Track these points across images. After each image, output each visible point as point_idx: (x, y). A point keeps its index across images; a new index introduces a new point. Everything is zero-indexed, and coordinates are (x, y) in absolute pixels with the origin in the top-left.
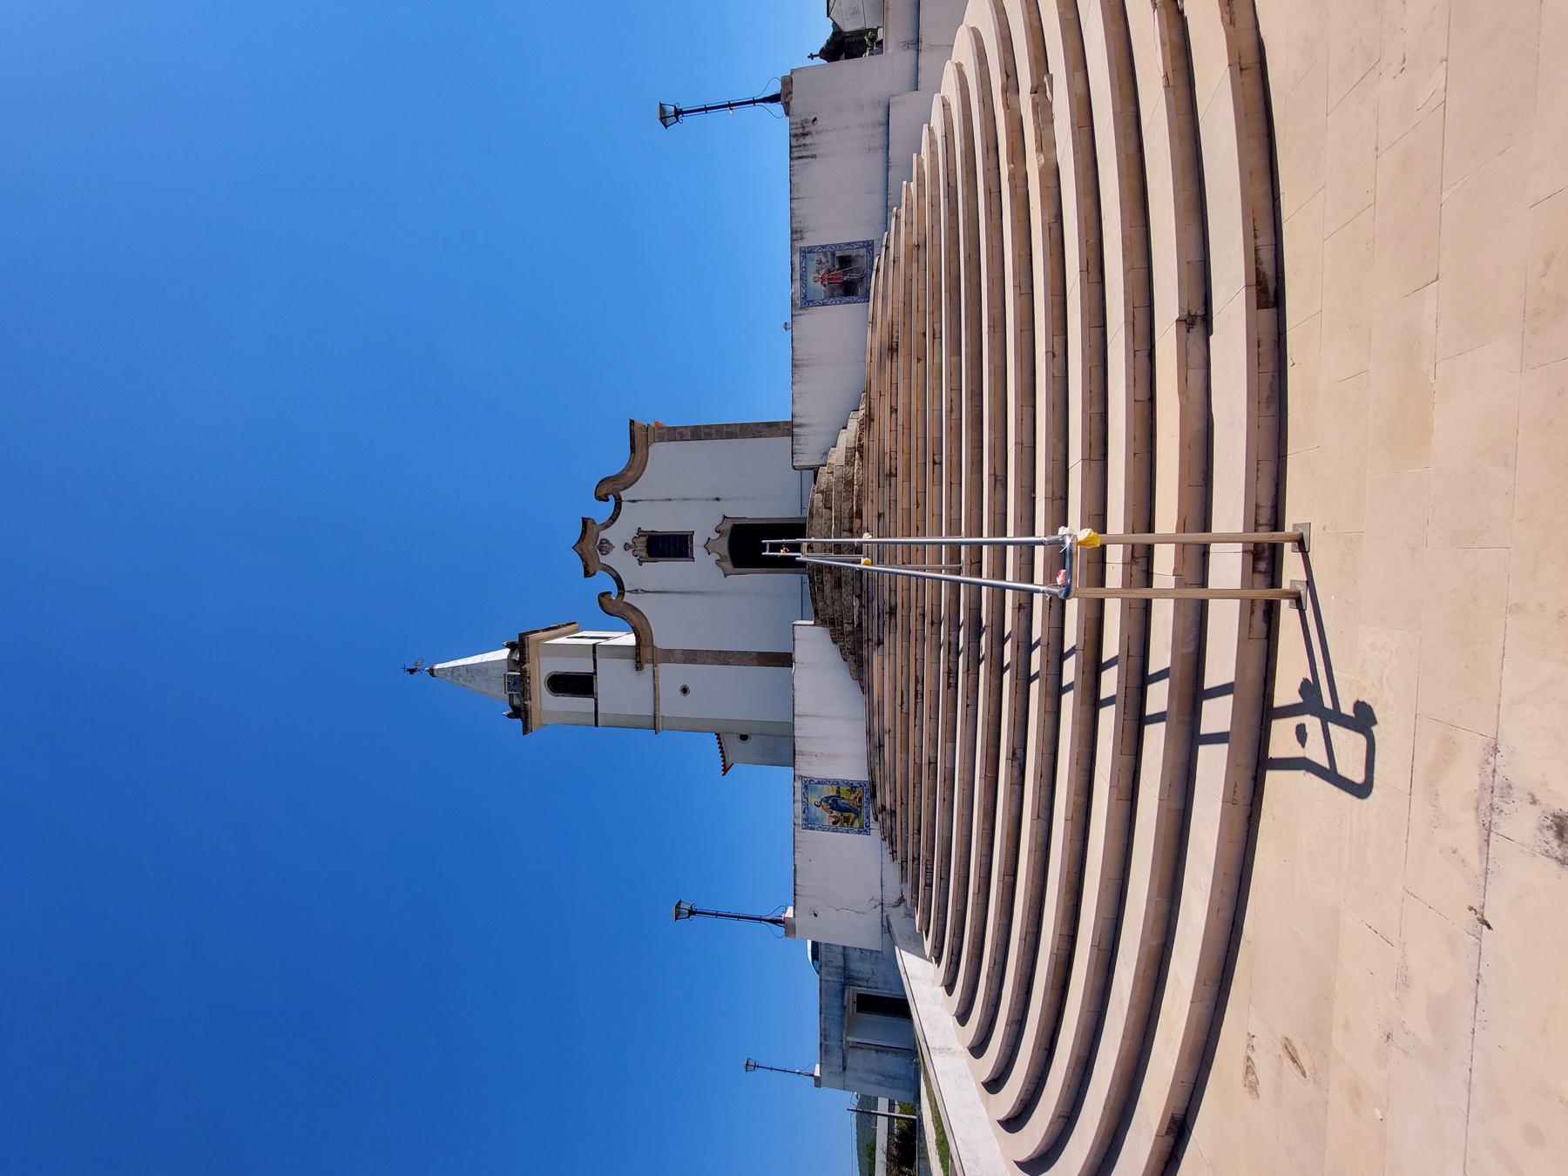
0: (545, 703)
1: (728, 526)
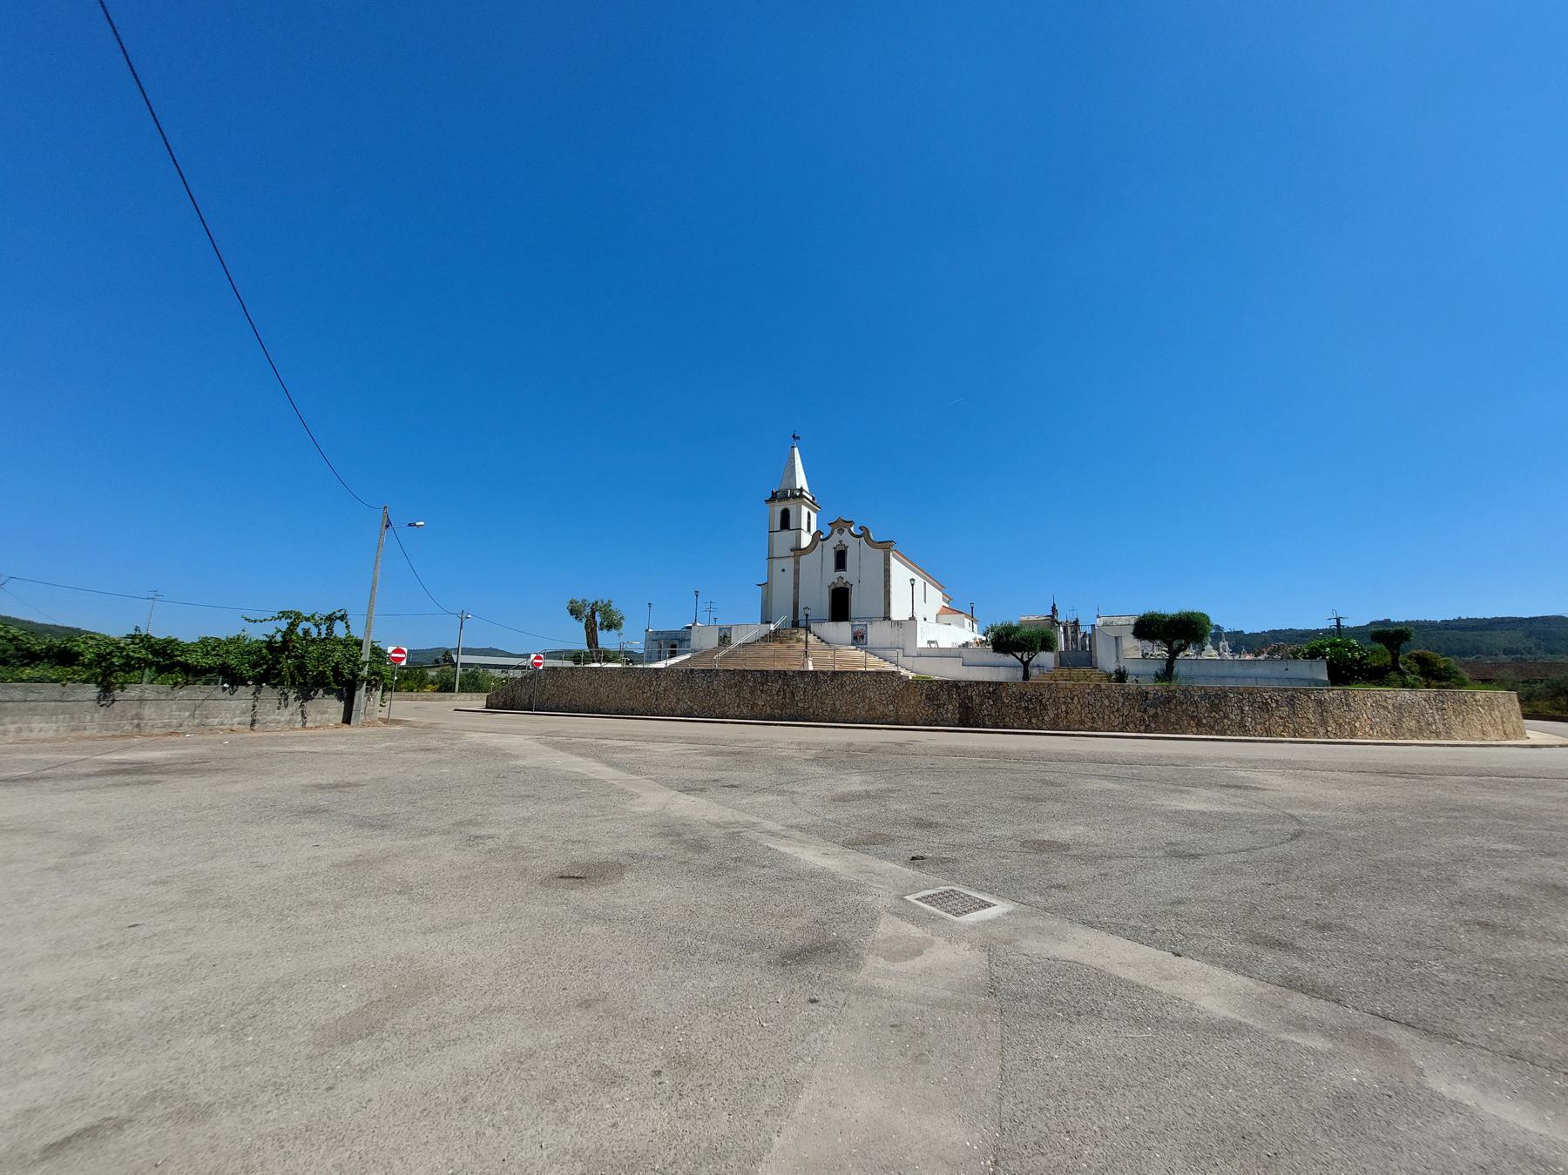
0: (778, 508)
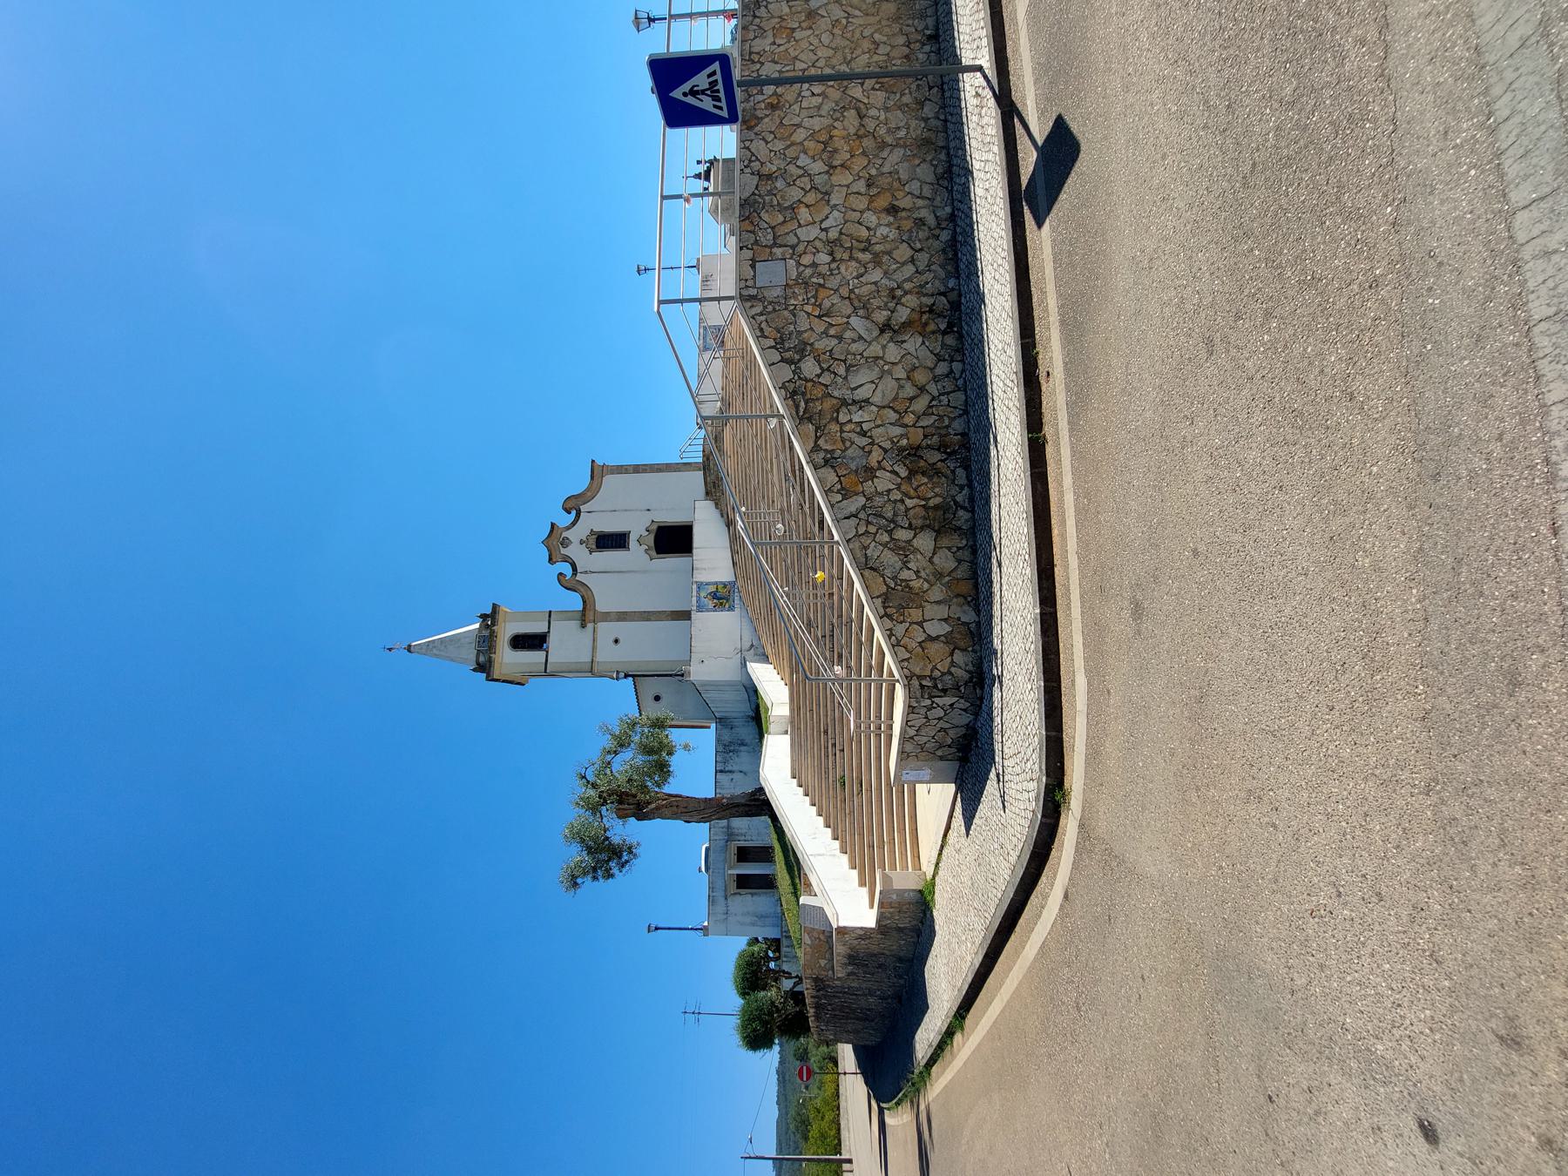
1: (655, 527)
